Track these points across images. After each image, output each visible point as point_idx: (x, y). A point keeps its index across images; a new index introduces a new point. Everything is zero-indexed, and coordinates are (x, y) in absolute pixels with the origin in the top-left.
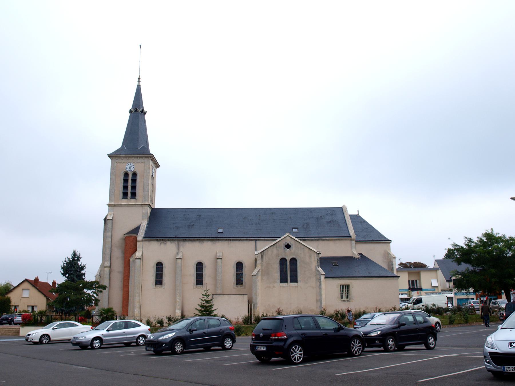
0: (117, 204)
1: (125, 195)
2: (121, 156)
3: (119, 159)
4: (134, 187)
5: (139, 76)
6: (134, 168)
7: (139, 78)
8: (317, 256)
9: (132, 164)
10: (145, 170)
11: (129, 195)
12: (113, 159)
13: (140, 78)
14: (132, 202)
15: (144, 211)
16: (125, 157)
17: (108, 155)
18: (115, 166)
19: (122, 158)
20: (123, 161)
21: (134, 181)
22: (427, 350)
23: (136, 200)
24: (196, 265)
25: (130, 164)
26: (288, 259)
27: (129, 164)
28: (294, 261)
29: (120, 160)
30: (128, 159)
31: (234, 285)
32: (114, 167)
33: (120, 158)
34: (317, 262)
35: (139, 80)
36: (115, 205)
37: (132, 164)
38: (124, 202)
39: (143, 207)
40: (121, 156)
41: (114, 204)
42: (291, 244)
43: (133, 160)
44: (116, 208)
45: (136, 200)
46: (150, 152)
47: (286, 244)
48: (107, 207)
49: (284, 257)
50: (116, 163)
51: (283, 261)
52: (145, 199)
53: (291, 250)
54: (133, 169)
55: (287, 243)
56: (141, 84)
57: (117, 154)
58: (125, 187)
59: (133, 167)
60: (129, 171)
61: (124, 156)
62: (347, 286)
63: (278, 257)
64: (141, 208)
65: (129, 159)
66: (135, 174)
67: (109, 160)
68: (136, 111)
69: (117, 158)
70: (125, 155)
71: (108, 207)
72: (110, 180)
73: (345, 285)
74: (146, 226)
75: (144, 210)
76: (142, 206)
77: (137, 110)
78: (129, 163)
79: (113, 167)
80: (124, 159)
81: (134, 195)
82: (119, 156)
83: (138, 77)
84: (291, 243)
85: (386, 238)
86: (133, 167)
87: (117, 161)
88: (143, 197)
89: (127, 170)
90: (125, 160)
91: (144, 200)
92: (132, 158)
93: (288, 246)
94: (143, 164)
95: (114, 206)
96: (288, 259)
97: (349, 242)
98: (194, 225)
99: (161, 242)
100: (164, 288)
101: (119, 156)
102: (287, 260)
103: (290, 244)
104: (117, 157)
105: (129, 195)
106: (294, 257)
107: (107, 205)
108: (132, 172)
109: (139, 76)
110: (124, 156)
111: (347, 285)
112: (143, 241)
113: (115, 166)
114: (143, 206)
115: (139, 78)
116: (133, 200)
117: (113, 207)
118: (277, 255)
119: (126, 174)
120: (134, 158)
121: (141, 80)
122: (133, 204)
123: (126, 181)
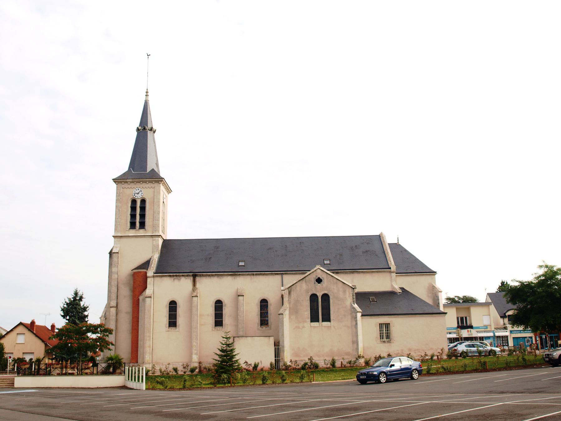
1: (133, 225)
4: (143, 216)
7: (147, 92)
8: (351, 291)
11: (138, 224)
14: (142, 232)
21: (143, 208)
24: (215, 304)
26: (320, 295)
28: (326, 297)
31: (258, 326)
32: (120, 193)
35: (147, 94)
37: (140, 189)
38: (132, 233)
39: (154, 238)
42: (322, 278)
49: (315, 293)
51: (313, 298)
53: (322, 285)
54: (141, 195)
55: (318, 277)
56: (150, 98)
58: (133, 216)
60: (137, 198)
62: (387, 325)
63: (308, 293)
66: (143, 201)
73: (385, 324)
79: (119, 193)
81: (143, 225)
83: (146, 91)
84: (323, 277)
89: (135, 196)
93: (319, 281)
96: (320, 295)
97: (388, 274)
99: (174, 278)
100: (178, 330)
102: (318, 296)
103: (321, 278)
105: (138, 224)
106: (326, 292)
109: (147, 89)
111: (387, 324)
112: (154, 277)
115: (147, 92)
118: (307, 291)
119: (134, 202)
121: (149, 94)
123: (133, 208)
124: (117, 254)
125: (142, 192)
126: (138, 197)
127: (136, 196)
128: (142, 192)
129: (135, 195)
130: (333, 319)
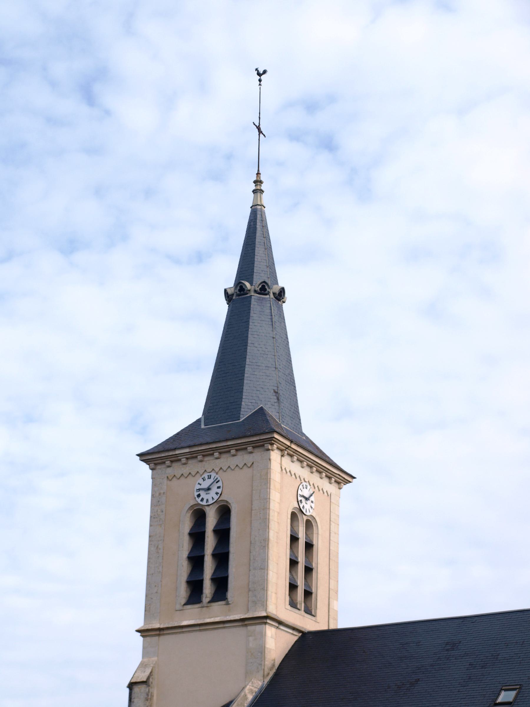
0: (166, 625)
2: (177, 452)
3: (174, 464)
5: (258, 174)
6: (219, 491)
7: (258, 182)
9: (213, 475)
10: (254, 492)
12: (159, 467)
13: (262, 179)
15: (251, 645)
16: (192, 456)
17: (138, 455)
18: (162, 492)
19: (184, 460)
20: (185, 470)
22: (130, 682)
23: (228, 604)
25: (210, 478)
29: (177, 469)
30: (201, 461)
33: (176, 460)
35: (258, 187)
36: (160, 629)
37: (213, 475)
39: (249, 628)
40: (177, 452)
41: (157, 626)
43: (218, 461)
44: (167, 640)
45: (228, 604)
46: (305, 430)
48: (139, 639)
50: (165, 480)
52: (255, 596)
54: (217, 493)
56: (266, 199)
57: (172, 447)
59: (219, 487)
60: (204, 503)
61: (187, 450)
64: (240, 632)
65: (206, 459)
67: (145, 470)
68: (240, 290)
69: (168, 463)
70: (189, 447)
71: (141, 639)
72: (150, 541)
74: (250, 697)
75: (251, 639)
76: (246, 625)
77: (266, 290)
78: (206, 475)
79: (157, 494)
80: (190, 462)
82: (171, 453)
85: (144, 462)
86: (219, 487)
87: (170, 472)
88: (249, 590)
90: (193, 466)
91: (253, 602)
92: (213, 454)
94: (250, 470)
95: (159, 635)
98: (418, 680)
101: (171, 453)
104: (167, 457)
107: (138, 631)
108: (216, 506)
109: (258, 174)
110: (187, 450)
113: (162, 492)
114: (246, 623)
115: (258, 182)
116: (218, 606)
117: (157, 638)
120: (220, 453)
121: (263, 187)
122: (217, 619)
126: (207, 501)
127: (202, 500)
128: (220, 484)
129: (199, 496)
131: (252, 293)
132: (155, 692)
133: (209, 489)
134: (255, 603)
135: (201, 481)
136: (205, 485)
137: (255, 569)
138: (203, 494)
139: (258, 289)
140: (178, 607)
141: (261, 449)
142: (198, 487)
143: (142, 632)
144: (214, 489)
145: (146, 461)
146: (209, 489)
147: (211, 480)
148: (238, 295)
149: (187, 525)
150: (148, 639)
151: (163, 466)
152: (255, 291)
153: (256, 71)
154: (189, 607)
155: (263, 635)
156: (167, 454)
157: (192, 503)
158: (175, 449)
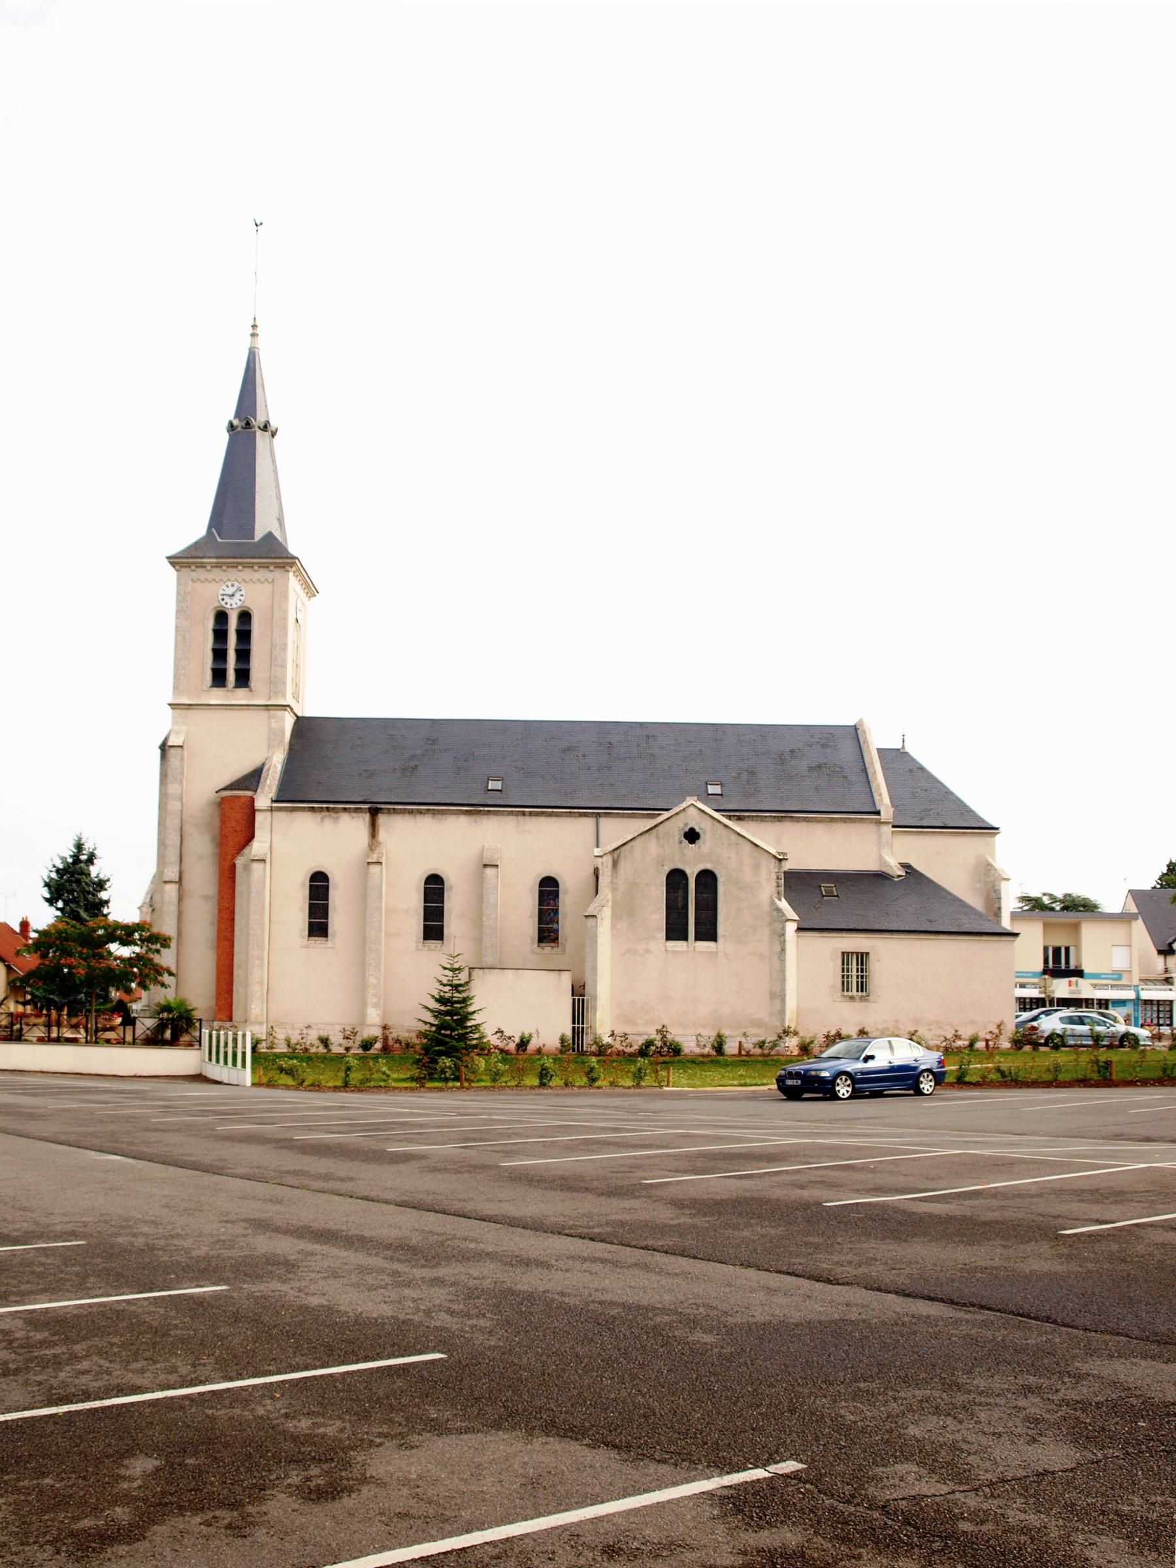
1: (219, 678)
2: (205, 560)
4: (244, 655)
6: (242, 598)
7: (254, 326)
9: (236, 584)
11: (231, 676)
12: (183, 569)
13: (257, 324)
14: (241, 696)
20: (210, 576)
21: (244, 635)
24: (425, 884)
25: (233, 586)
26: (692, 873)
27: (227, 586)
28: (707, 879)
29: (201, 574)
31: (533, 943)
34: (775, 884)
38: (218, 696)
39: (271, 712)
44: (194, 715)
45: (251, 691)
47: (687, 830)
49: (679, 866)
50: (190, 583)
51: (676, 879)
53: (699, 848)
55: (689, 827)
56: (260, 343)
58: (219, 654)
60: (228, 606)
61: (214, 560)
62: (862, 957)
64: (263, 715)
66: (245, 617)
67: (171, 573)
70: (217, 558)
73: (857, 954)
78: (229, 584)
81: (243, 678)
83: (252, 323)
87: (194, 574)
89: (223, 603)
90: (216, 574)
94: (271, 586)
96: (692, 873)
102: (689, 875)
103: (697, 830)
104: (193, 563)
105: (231, 676)
106: (708, 866)
107: (170, 705)
108: (239, 610)
112: (271, 810)
115: (254, 326)
116: (242, 692)
119: (221, 617)
123: (220, 634)
124: (179, 750)
125: (242, 593)
128: (242, 593)
130: (724, 936)
131: (257, 429)
132: (185, 753)
133: (233, 595)
134: (276, 693)
135: (225, 587)
136: (230, 591)
137: (276, 666)
138: (227, 599)
139: (262, 426)
140: (205, 688)
141: (282, 570)
142: (222, 592)
143: (173, 706)
144: (238, 596)
145: (173, 564)
146: (233, 595)
147: (234, 589)
148: (243, 428)
149: (210, 624)
150: (178, 711)
151: (188, 569)
152: (259, 428)
153: (907, 867)
154: (238, 690)
155: (283, 719)
156: (194, 560)
157: (217, 604)
158: (203, 557)
